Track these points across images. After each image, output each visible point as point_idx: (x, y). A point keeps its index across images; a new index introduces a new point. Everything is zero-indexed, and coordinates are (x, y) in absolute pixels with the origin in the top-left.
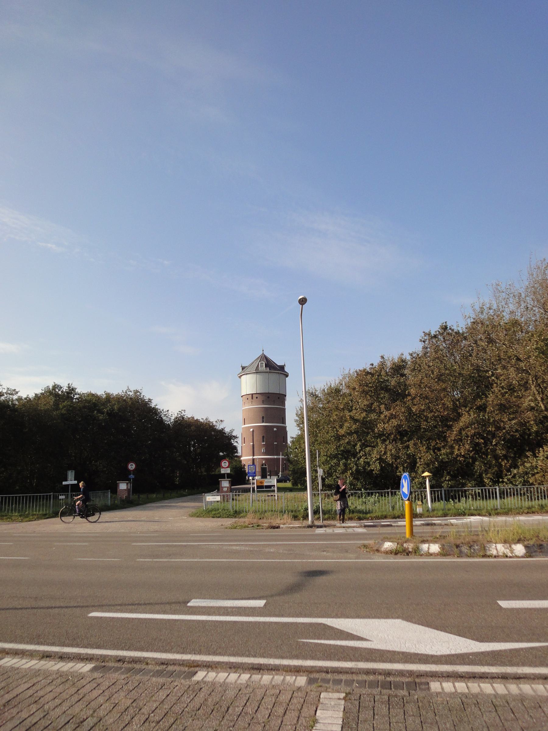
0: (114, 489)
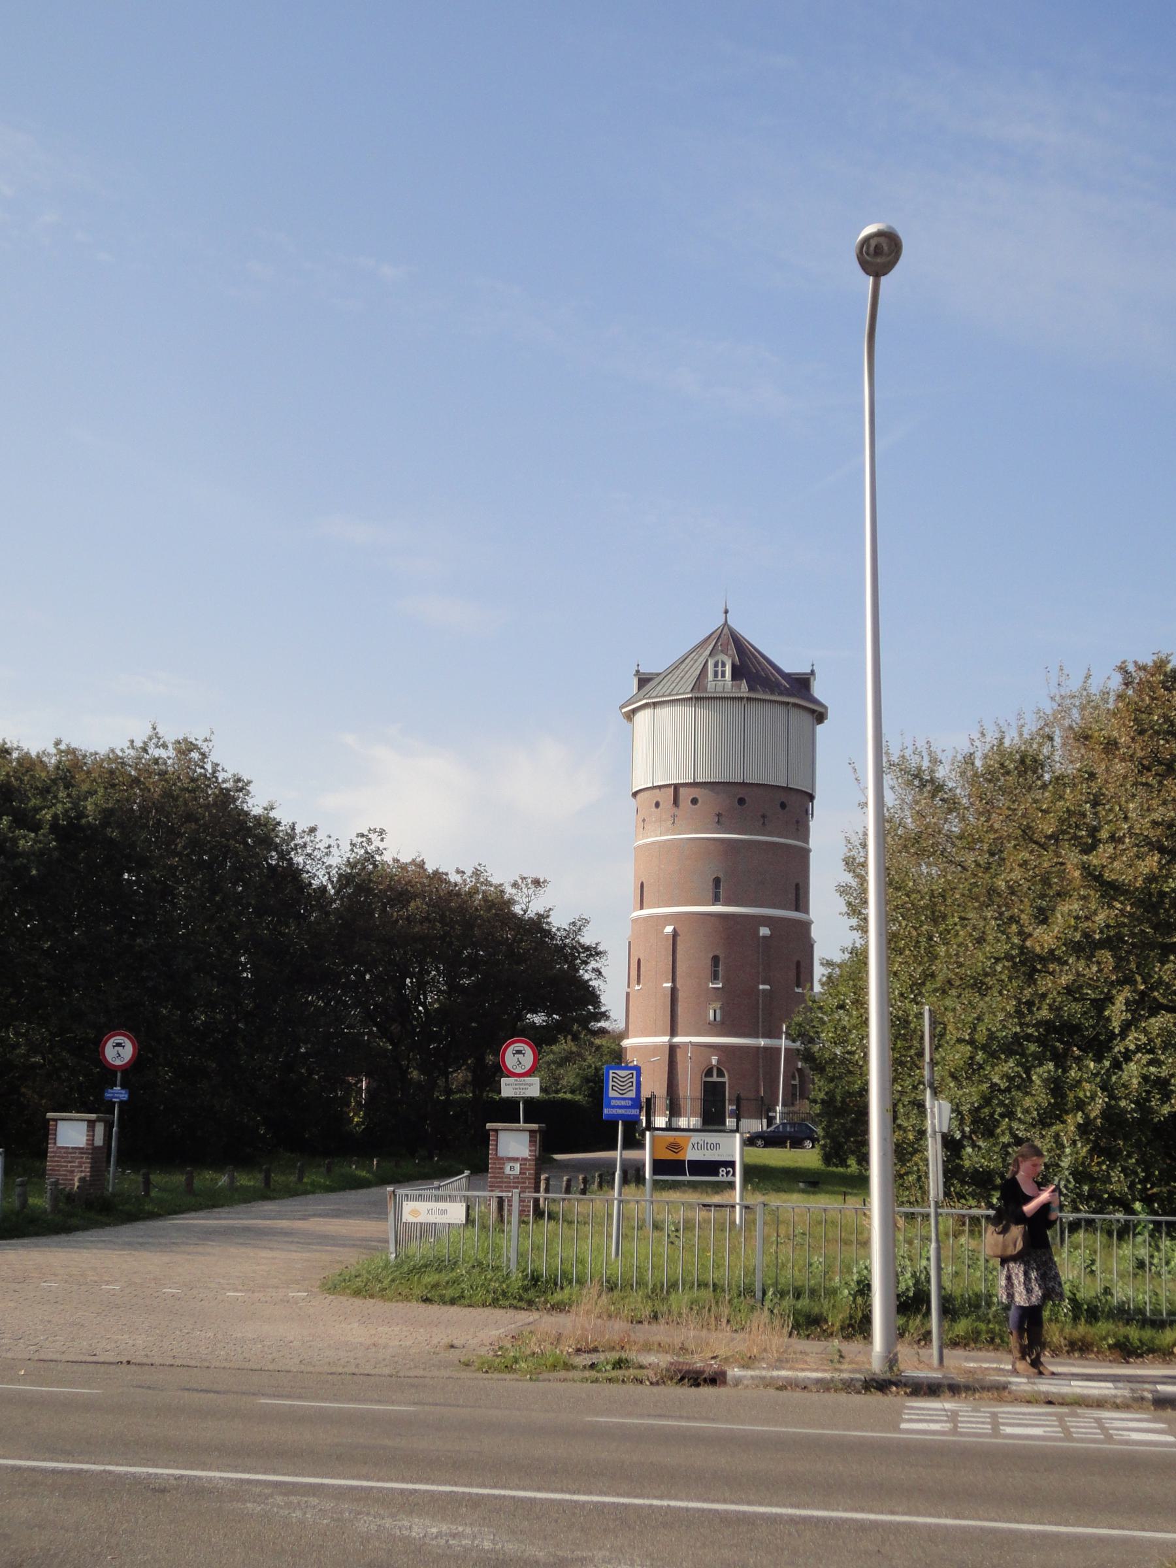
0: (31, 1145)
